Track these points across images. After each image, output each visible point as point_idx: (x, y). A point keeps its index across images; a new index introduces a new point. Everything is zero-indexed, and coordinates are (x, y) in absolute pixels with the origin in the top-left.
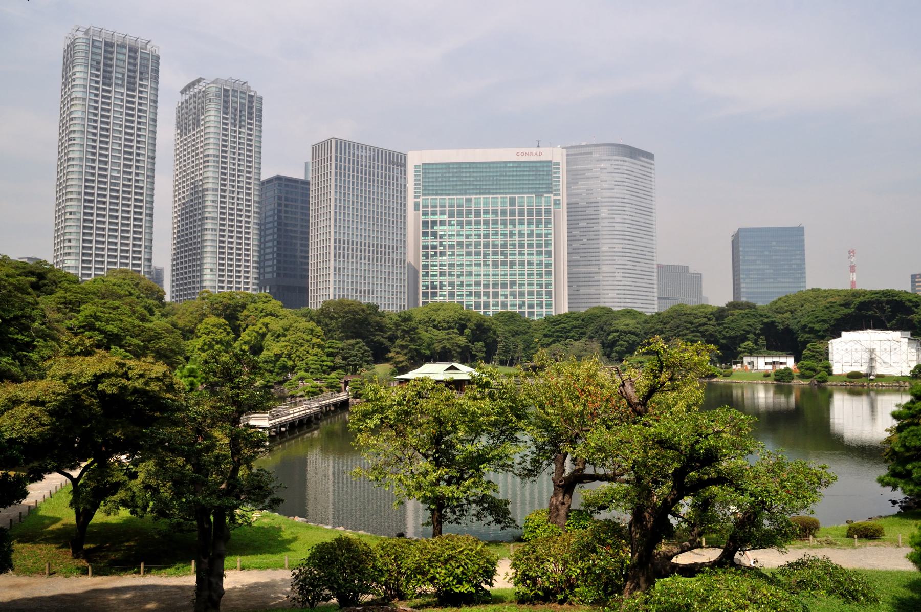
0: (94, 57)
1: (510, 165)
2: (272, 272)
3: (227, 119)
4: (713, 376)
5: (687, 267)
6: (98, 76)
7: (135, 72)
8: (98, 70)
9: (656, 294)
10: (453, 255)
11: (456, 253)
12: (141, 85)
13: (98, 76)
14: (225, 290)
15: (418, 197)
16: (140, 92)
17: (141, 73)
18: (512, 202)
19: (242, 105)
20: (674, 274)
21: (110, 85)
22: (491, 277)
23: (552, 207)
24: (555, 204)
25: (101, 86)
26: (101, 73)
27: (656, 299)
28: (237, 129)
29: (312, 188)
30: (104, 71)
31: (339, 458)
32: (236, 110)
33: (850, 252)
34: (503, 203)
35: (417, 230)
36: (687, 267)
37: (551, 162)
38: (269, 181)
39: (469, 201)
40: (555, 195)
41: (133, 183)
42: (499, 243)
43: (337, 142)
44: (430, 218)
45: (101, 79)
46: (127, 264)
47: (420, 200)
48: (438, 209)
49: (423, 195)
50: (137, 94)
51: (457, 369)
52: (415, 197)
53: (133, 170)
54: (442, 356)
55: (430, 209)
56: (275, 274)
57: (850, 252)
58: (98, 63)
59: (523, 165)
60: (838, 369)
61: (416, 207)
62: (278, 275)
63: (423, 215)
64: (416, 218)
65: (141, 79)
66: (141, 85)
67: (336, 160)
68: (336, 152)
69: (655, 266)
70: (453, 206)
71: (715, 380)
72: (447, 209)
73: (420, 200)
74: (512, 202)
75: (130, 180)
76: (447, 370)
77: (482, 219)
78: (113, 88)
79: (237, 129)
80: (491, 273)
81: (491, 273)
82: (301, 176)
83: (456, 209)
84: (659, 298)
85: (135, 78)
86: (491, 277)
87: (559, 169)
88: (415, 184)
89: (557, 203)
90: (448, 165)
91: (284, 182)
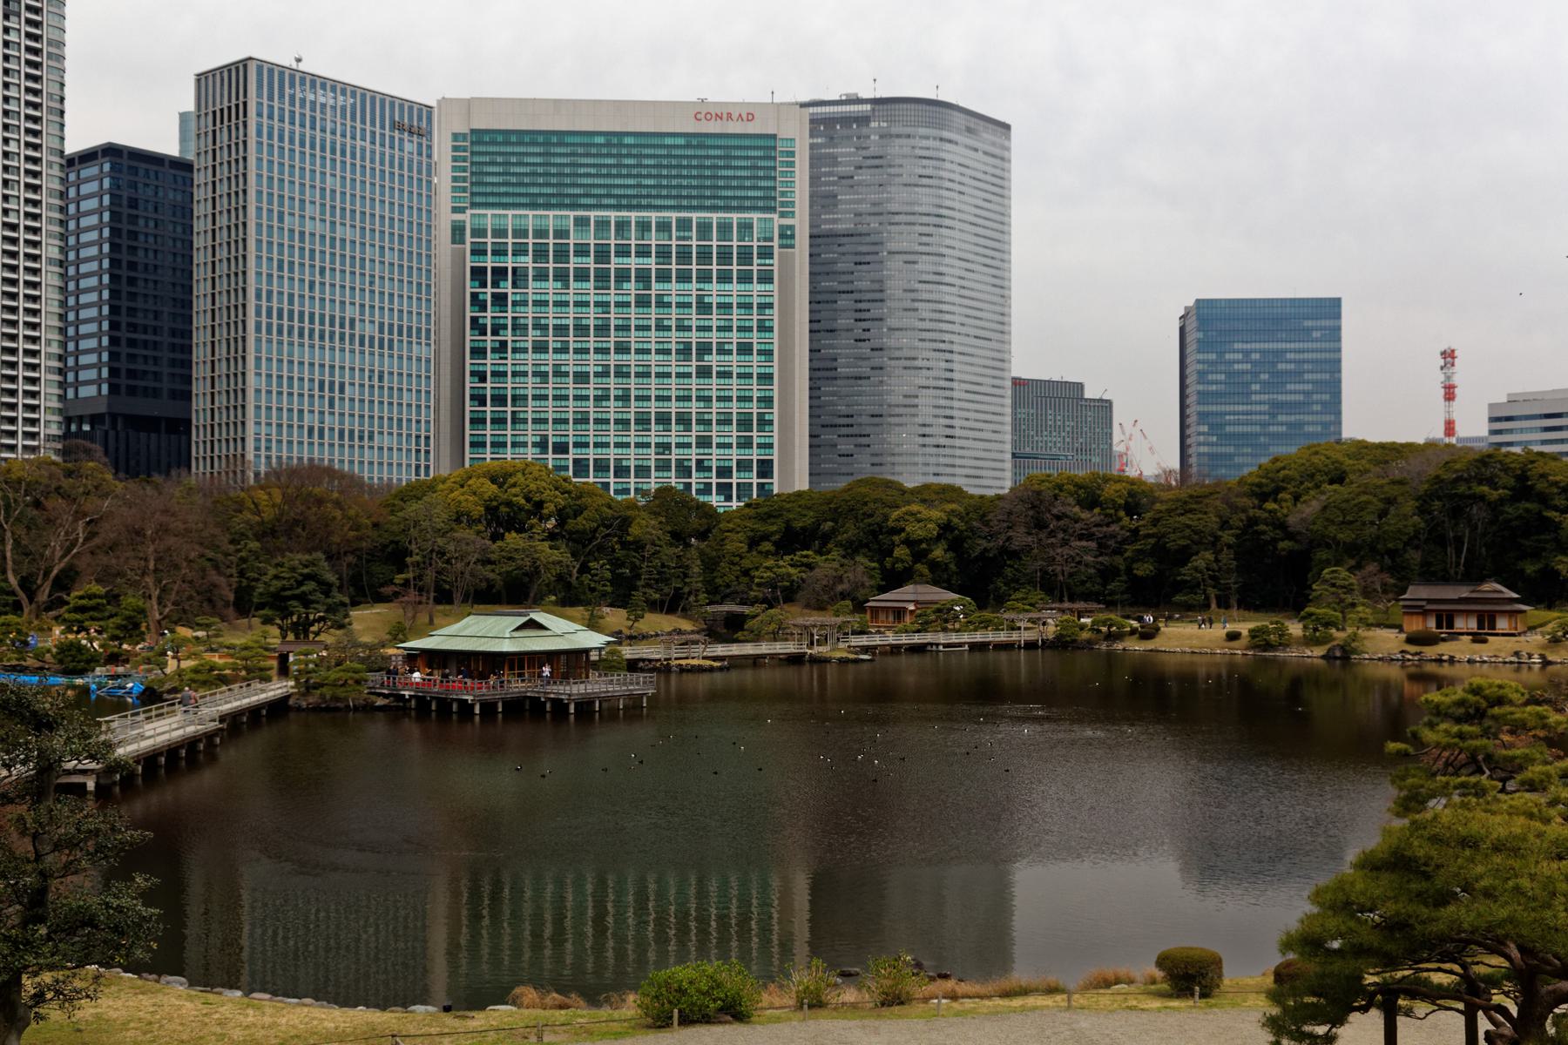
1: (628, 140)
2: (98, 382)
4: (1119, 637)
5: (1080, 386)
9: (1008, 447)
10: (564, 350)
11: (572, 346)
15: (461, 210)
20: (1059, 406)
22: (734, 403)
23: (776, 243)
24: (782, 236)
27: (1009, 456)
29: (199, 178)
33: (1444, 354)
35: (459, 288)
36: (1080, 386)
37: (774, 137)
38: (88, 157)
40: (783, 215)
42: (592, 323)
43: (260, 69)
44: (489, 262)
47: (466, 217)
49: (474, 205)
51: (541, 627)
52: (455, 210)
54: (489, 597)
55: (510, 240)
56: (105, 389)
57: (1444, 354)
59: (709, 142)
61: (458, 232)
62: (114, 389)
63: (474, 252)
64: (459, 260)
67: (260, 115)
68: (260, 95)
69: (1009, 384)
70: (524, 233)
71: (1119, 646)
72: (530, 241)
73: (466, 217)
76: (517, 629)
77: (571, 266)
80: (571, 393)
81: (571, 393)
82: (169, 146)
83: (510, 240)
84: (1014, 455)
86: (734, 403)
88: (455, 179)
89: (787, 235)
91: (125, 162)
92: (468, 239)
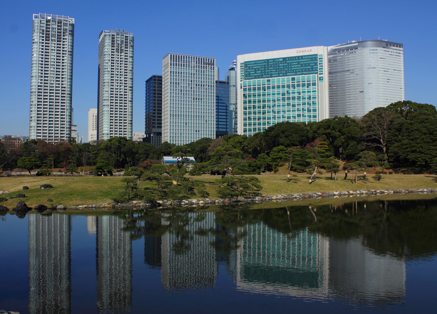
0: (41, 28)
1: (258, 62)
3: (114, 50)
6: (43, 37)
7: (61, 32)
8: (43, 34)
12: (64, 39)
13: (43, 37)
14: (118, 136)
16: (64, 42)
17: (64, 33)
18: (293, 79)
19: (122, 42)
21: (49, 40)
25: (44, 42)
26: (44, 35)
28: (119, 54)
30: (46, 34)
31: (203, 229)
32: (119, 44)
34: (288, 81)
37: (317, 55)
39: (269, 81)
41: (60, 86)
45: (44, 38)
46: (121, 134)
48: (252, 87)
50: (62, 43)
53: (60, 79)
58: (43, 31)
60: (242, 134)
65: (64, 36)
66: (64, 39)
73: (242, 82)
74: (293, 79)
75: (59, 84)
78: (50, 42)
79: (119, 54)
85: (61, 35)
87: (241, 67)
90: (267, 61)
92: (243, 87)
